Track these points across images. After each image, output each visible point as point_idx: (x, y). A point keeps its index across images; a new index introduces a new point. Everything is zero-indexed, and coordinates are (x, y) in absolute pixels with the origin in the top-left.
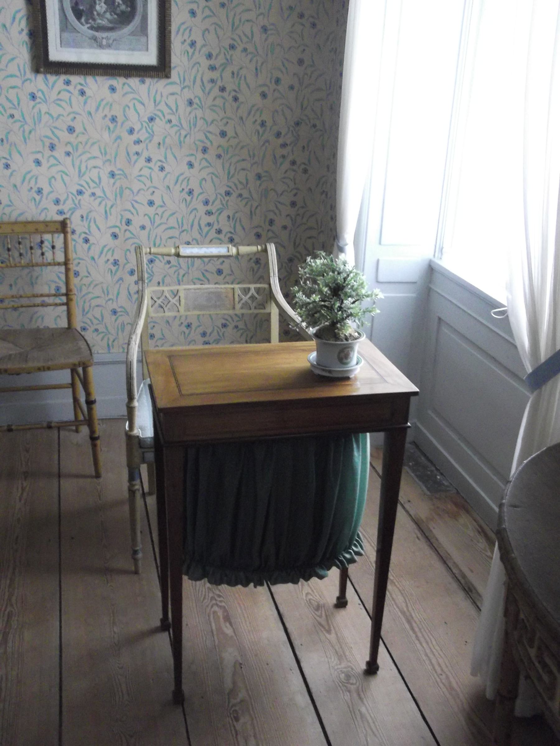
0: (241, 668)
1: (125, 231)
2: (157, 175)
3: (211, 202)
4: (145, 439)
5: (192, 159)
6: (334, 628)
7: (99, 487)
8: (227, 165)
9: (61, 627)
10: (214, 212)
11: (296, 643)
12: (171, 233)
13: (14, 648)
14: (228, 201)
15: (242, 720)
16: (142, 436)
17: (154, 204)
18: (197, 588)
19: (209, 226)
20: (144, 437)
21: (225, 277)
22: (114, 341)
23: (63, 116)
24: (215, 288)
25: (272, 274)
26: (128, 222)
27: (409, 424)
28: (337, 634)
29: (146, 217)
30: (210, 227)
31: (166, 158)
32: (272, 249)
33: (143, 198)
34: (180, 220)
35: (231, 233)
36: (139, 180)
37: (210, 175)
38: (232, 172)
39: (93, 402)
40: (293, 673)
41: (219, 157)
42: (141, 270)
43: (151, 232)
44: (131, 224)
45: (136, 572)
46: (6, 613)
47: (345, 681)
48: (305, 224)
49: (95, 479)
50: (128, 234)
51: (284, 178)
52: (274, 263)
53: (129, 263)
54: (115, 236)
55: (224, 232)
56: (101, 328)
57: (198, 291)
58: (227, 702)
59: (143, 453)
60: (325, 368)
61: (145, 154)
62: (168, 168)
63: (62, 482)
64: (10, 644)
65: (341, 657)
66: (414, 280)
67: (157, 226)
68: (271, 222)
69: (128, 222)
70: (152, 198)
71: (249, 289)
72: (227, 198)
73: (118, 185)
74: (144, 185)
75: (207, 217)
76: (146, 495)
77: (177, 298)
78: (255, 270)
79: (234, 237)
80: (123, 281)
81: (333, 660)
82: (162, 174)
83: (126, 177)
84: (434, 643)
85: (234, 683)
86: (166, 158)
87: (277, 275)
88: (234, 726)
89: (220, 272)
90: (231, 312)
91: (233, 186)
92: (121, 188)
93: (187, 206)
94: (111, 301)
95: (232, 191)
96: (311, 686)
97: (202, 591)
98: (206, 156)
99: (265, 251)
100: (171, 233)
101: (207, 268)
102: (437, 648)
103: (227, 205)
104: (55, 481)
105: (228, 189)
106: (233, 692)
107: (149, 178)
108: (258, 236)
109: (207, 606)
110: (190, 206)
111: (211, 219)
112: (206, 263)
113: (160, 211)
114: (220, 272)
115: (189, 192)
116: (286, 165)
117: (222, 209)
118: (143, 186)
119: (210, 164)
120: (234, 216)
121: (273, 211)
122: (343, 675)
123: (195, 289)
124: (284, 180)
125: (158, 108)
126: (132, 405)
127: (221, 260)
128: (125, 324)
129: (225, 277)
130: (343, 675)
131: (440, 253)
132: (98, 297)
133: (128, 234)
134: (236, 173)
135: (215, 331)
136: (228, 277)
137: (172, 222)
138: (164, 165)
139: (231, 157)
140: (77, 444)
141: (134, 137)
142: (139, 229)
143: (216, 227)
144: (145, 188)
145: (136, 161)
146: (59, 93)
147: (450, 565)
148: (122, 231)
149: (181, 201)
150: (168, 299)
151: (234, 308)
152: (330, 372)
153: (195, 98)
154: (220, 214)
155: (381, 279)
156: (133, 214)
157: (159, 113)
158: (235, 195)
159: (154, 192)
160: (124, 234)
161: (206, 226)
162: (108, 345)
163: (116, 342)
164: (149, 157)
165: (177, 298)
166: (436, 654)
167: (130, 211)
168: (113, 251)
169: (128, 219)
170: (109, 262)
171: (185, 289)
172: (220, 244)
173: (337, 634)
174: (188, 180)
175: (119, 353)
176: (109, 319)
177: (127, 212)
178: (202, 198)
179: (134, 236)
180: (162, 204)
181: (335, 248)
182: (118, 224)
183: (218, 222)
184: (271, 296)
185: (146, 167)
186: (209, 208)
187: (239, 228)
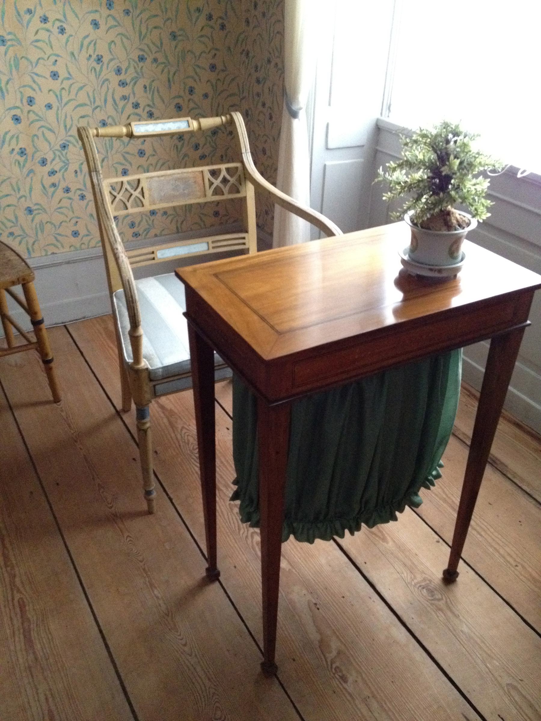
0: (318, 609)
1: (29, 112)
2: (58, 40)
3: (124, 70)
4: (156, 371)
5: (96, 16)
6: (388, 534)
7: (63, 414)
8: (137, 23)
9: (90, 605)
10: (141, 233)
11: (359, 561)
12: (82, 111)
13: (45, 651)
14: (142, 67)
15: (350, 679)
16: (151, 367)
17: (59, 77)
18: (226, 517)
19: (125, 100)
20: (153, 368)
21: (148, 158)
22: (33, 244)
23: (43, 59)
24: (182, 173)
25: (243, 150)
26: (31, 101)
27: (528, 322)
28: (394, 542)
29: (51, 92)
30: (126, 101)
31: (65, 16)
32: (239, 119)
33: (44, 70)
34: (91, 94)
35: (149, 105)
36: (36, 46)
37: (119, 37)
38: (144, 31)
39: (41, 322)
40: (374, 601)
41: (127, 13)
42: (92, 159)
43: (59, 112)
44: (34, 104)
45: (150, 512)
46: (16, 604)
47: (430, 598)
48: (226, 90)
49: (55, 405)
50: (32, 116)
51: (202, 36)
52: (244, 136)
53: (38, 151)
54: (17, 119)
55: (142, 106)
56: (17, 231)
57: (162, 178)
58: (324, 659)
59: (154, 386)
60: (432, 267)
61: (63, 185)
62: (69, 30)
63: (16, 414)
64: (38, 646)
65: (411, 569)
66: (362, 144)
67: (66, 104)
68: (191, 91)
69: (31, 101)
70: (55, 69)
71: (220, 170)
72: (141, 64)
73: (11, 53)
74: (43, 53)
75: (121, 89)
76: (121, 414)
77: (139, 189)
78: (179, 147)
79: (153, 110)
80: (35, 174)
81: (405, 575)
82: (64, 38)
83: (20, 43)
84: (492, 530)
85: (319, 631)
86: (65, 16)
87: (249, 151)
88: (345, 689)
89: (142, 153)
90: (202, 200)
91: (146, 49)
92: (16, 58)
93: (98, 77)
94: (23, 199)
95: (146, 56)
96: (399, 613)
97: (233, 519)
98: (112, 12)
99: (232, 122)
100: (82, 111)
101: (128, 149)
102: (496, 534)
103: (142, 72)
104: (8, 416)
105: (141, 53)
106: (323, 644)
107: (210, 38)
108: (179, 107)
109: (247, 537)
110: (101, 77)
111: (126, 91)
112: (126, 144)
113: (66, 84)
114: (142, 153)
115: (96, 59)
116: (202, 21)
117: (137, 77)
118: (42, 55)
119: (119, 23)
120: (151, 85)
121: (193, 77)
122: (424, 590)
123: (158, 177)
124: (202, 39)
125: (69, 134)
126: (138, 334)
127: (142, 140)
128: (44, 224)
129: (148, 158)
130: (424, 590)
131: (388, 111)
132: (7, 195)
133: (32, 116)
134: (149, 33)
135: (144, 220)
136: (151, 158)
137: (82, 97)
138: (65, 26)
139: (141, 13)
140: (16, 365)
141: (48, 168)
142: (44, 109)
143: (132, 100)
144: (46, 57)
145: (29, 22)
146: (37, 32)
147: (461, 436)
148: (26, 114)
149: (90, 70)
150: (129, 192)
151: (205, 196)
152: (440, 271)
153: (108, 118)
154: (135, 83)
155: (331, 146)
156: (34, 90)
157: (71, 139)
158: (149, 60)
159: (56, 61)
160: (28, 116)
161: (121, 99)
162: (28, 249)
163: (36, 244)
164: (45, 16)
165: (139, 189)
166: (500, 542)
167: (30, 87)
168: (18, 137)
169: (30, 97)
170: (15, 152)
171: (147, 178)
172: (139, 120)
173: (394, 542)
174: (95, 44)
175: (42, 256)
176: (24, 219)
177: (27, 88)
178: (113, 65)
179: (40, 119)
180: (67, 75)
181: (285, 112)
182: (18, 104)
183: (134, 94)
184: (246, 176)
185: (43, 29)
186: (122, 77)
187: (157, 100)
